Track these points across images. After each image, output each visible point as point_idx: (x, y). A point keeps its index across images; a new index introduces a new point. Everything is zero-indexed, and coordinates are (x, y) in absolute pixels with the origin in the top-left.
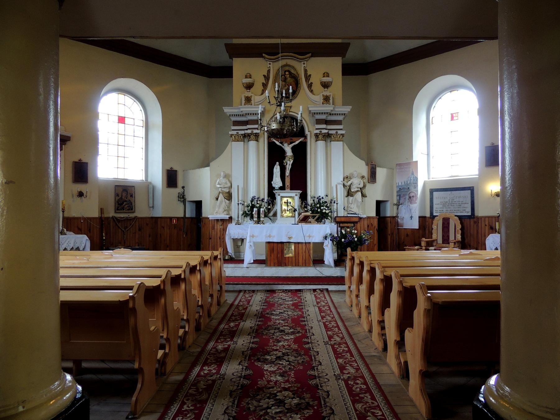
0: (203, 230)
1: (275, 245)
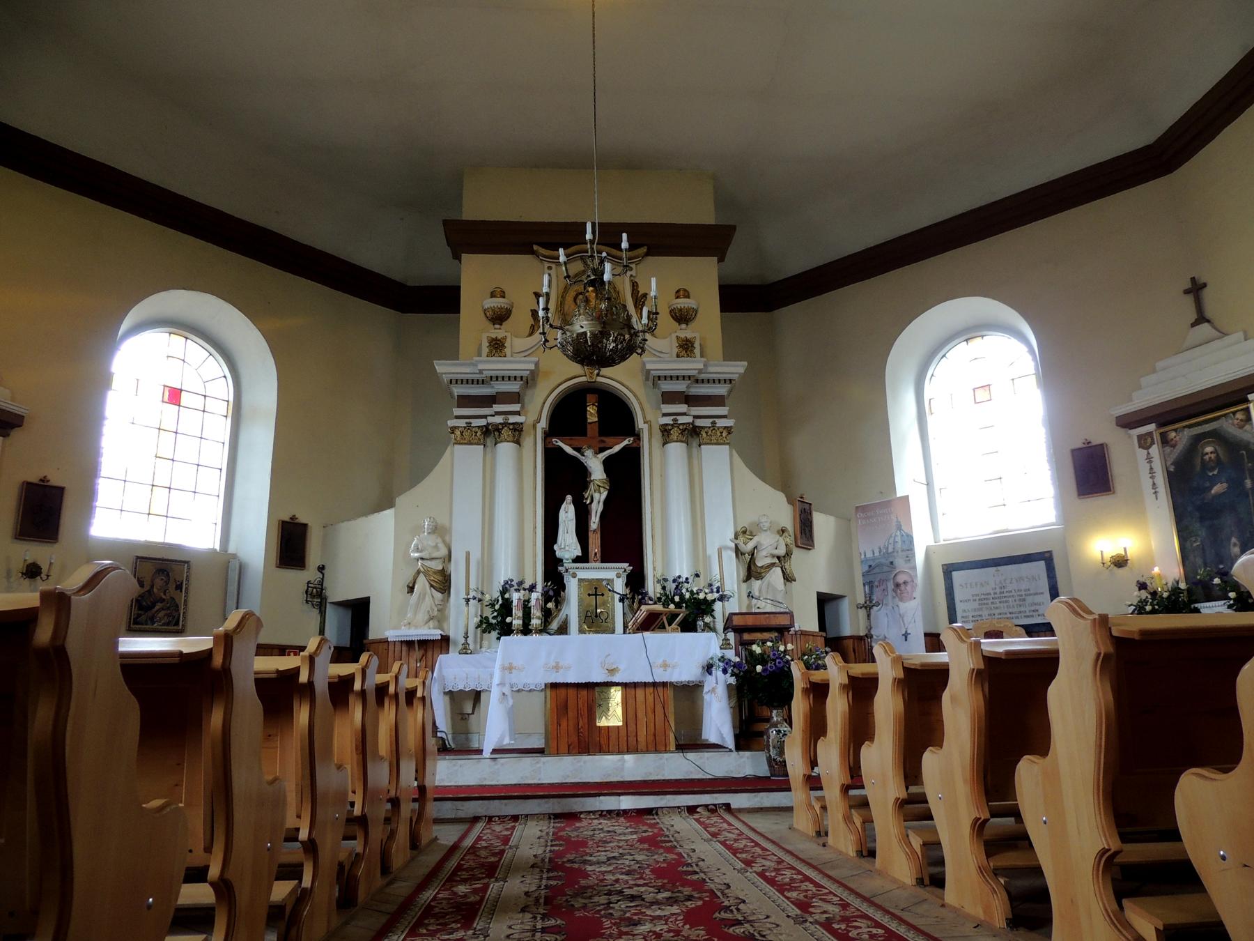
1: (572, 692)
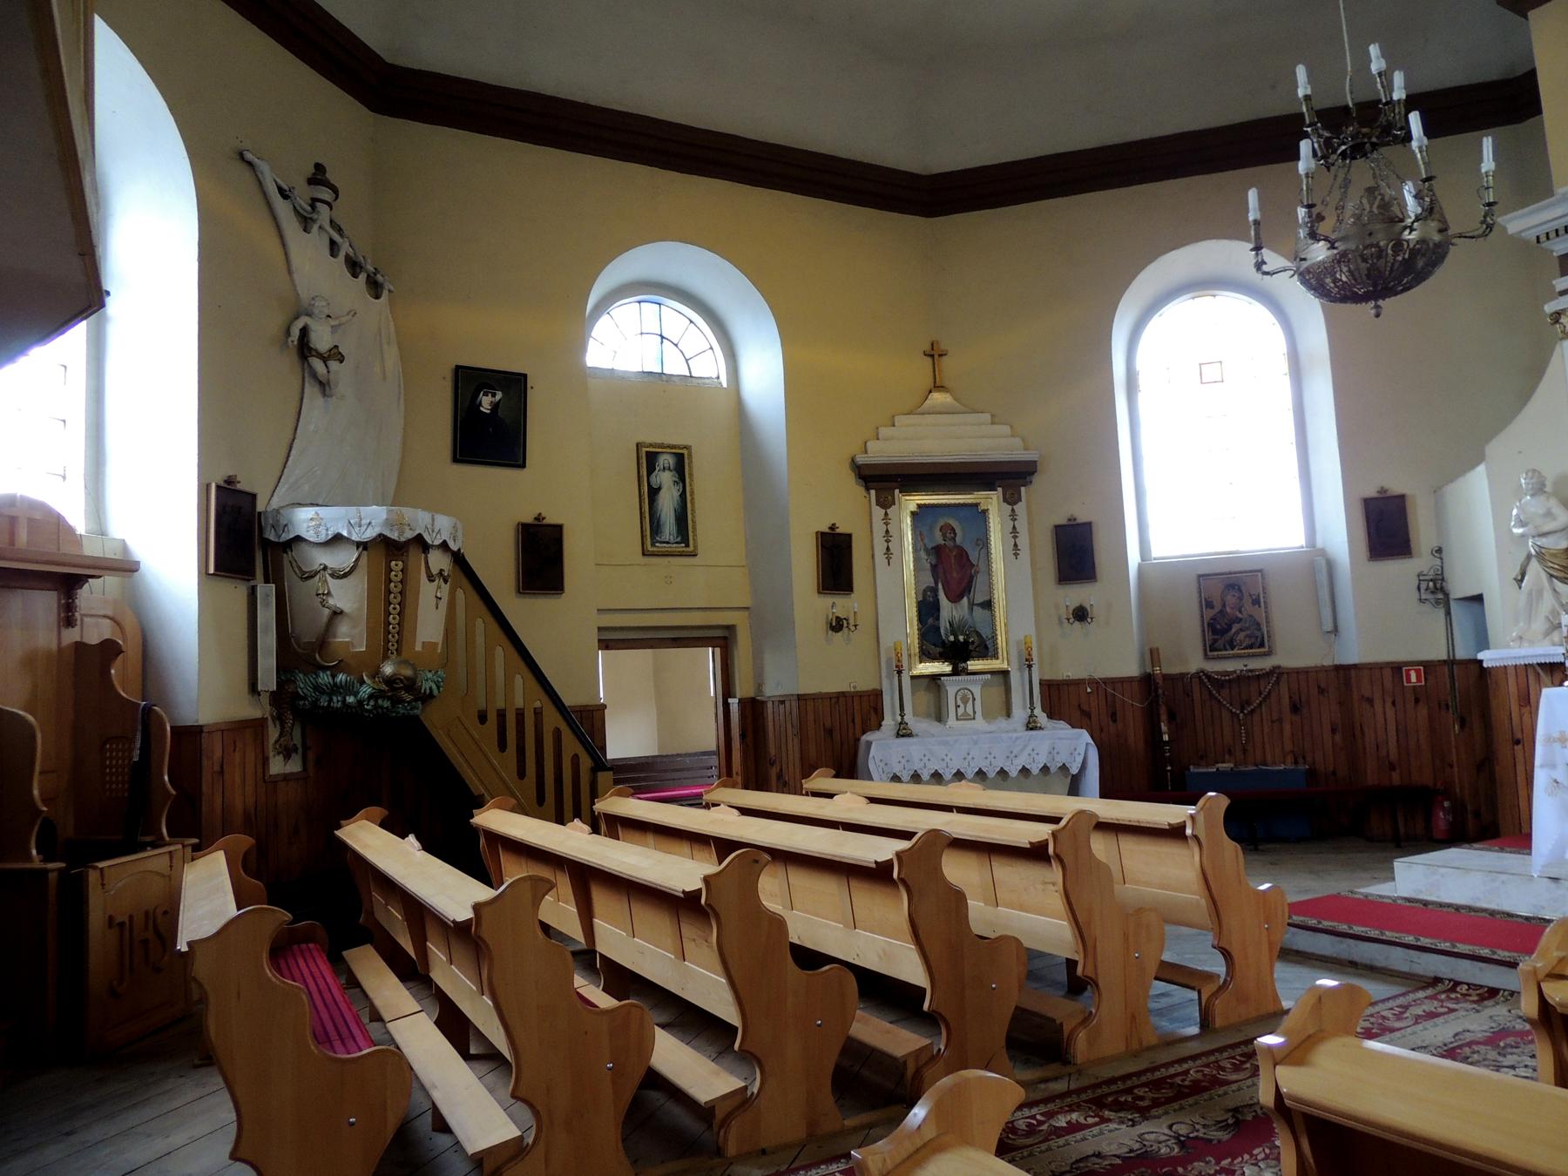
0: (1494, 703)
